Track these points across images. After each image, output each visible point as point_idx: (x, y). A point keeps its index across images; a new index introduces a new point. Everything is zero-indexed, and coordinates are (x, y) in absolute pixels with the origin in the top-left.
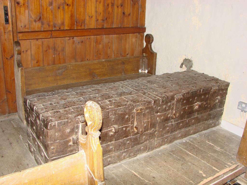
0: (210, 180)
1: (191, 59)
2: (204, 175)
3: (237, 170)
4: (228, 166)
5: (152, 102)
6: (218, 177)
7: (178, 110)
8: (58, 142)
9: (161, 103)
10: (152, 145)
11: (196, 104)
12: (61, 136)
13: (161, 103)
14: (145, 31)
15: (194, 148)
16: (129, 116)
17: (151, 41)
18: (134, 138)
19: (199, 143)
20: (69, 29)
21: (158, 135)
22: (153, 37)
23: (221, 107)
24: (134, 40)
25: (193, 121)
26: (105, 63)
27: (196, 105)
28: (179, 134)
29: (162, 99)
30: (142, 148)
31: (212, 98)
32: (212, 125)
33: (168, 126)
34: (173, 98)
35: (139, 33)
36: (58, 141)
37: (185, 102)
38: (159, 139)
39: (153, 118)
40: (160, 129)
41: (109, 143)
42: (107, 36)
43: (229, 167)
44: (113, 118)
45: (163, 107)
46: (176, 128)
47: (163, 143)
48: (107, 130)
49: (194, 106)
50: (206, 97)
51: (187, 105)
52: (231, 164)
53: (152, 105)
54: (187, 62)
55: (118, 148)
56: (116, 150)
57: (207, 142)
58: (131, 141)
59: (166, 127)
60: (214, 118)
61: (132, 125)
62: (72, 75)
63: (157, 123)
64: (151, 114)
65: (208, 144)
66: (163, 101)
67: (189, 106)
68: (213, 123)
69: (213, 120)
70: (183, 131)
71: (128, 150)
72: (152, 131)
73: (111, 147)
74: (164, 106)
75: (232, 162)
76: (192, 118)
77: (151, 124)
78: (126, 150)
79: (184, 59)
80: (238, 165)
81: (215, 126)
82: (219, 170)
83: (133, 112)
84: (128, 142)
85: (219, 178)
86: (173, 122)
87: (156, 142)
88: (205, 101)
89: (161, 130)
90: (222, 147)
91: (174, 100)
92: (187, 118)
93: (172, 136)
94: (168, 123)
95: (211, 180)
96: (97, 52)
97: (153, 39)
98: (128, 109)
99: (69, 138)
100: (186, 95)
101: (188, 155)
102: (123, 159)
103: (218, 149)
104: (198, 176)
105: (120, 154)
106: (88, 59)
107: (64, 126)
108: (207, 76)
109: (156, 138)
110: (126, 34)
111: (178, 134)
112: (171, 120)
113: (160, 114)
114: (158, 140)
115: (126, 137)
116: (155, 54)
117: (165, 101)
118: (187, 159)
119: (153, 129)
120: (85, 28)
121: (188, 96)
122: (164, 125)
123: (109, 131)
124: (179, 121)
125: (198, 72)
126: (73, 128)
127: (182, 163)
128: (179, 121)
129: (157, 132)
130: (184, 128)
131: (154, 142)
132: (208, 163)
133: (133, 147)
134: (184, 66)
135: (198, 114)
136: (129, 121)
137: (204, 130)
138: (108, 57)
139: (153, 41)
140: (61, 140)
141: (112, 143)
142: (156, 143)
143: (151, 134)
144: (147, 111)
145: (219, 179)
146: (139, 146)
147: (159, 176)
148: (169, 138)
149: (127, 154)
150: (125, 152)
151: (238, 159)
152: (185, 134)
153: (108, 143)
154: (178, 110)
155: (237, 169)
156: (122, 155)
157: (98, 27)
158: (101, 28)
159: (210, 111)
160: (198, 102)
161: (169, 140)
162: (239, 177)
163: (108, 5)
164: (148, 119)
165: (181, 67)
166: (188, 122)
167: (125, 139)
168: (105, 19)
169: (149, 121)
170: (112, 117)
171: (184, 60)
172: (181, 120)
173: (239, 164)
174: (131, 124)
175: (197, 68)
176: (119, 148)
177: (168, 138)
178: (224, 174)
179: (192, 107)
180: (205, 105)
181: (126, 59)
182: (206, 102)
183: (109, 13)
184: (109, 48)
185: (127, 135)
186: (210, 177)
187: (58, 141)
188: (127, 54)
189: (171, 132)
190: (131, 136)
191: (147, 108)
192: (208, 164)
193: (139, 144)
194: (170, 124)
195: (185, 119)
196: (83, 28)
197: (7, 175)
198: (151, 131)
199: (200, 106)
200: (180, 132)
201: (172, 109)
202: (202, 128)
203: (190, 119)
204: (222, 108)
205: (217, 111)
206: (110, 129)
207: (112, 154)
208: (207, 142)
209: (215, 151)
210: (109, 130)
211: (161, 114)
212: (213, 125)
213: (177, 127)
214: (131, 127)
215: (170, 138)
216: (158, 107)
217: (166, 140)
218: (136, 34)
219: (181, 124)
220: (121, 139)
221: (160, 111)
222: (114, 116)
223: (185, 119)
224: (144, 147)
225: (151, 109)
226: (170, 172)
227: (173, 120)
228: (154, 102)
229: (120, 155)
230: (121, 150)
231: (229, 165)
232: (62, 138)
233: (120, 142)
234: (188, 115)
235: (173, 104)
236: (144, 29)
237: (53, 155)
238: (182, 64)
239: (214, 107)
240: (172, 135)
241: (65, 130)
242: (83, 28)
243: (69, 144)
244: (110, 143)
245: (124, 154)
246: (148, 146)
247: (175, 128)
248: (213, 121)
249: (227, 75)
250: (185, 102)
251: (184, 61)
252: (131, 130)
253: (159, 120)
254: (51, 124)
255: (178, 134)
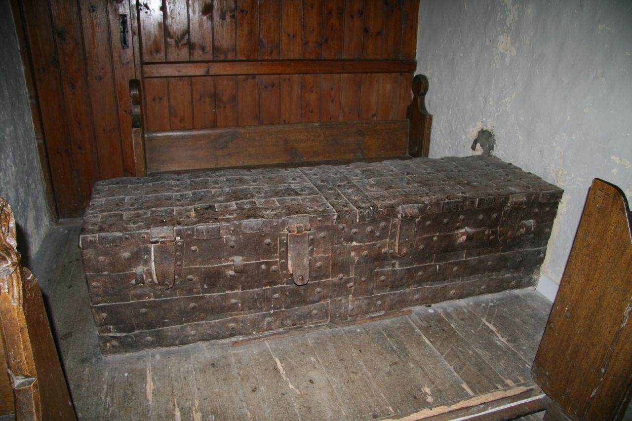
0: (439, 415)
1: (492, 130)
2: (430, 399)
3: (536, 397)
4: (503, 388)
5: (334, 215)
6: (467, 408)
7: (407, 239)
8: (105, 275)
9: (358, 220)
10: (342, 309)
11: (463, 231)
12: (112, 264)
13: (359, 221)
14: (414, 69)
15: (444, 330)
16: (274, 239)
17: (422, 91)
18: (290, 289)
19: (463, 320)
20: (244, 58)
21: (355, 290)
22: (427, 83)
23: (539, 245)
24: (388, 87)
25: (455, 269)
26: (319, 130)
27: (463, 234)
28: (417, 294)
29: (361, 212)
30: (315, 312)
31: (510, 222)
32: (510, 282)
33: (382, 274)
34: (391, 212)
35: (401, 73)
36: (106, 273)
37: (428, 223)
38: (360, 299)
39: (338, 252)
40: (361, 277)
41: (227, 292)
42: (328, 76)
43: (505, 390)
44: (231, 241)
45: (365, 229)
46: (404, 281)
47: (370, 308)
48: (219, 265)
49: (456, 234)
50: (492, 218)
51: (436, 233)
52: (513, 384)
53: (332, 222)
54: (485, 138)
55: (252, 304)
56: (247, 309)
57: (484, 320)
58: (284, 294)
59: (378, 275)
60: (517, 268)
61: (283, 261)
62: (246, 150)
63: (352, 263)
64: (332, 243)
65: (483, 326)
66: (362, 218)
67: (442, 234)
68: (513, 278)
69: (514, 272)
70: (426, 289)
71: (277, 312)
72: (338, 278)
73: (233, 301)
74: (369, 229)
75: (520, 378)
76: (450, 261)
77: (334, 265)
78: (273, 311)
79: (480, 130)
80: (532, 390)
81: (519, 286)
82: (473, 390)
83: (282, 233)
84: (276, 295)
85: (470, 411)
86: (397, 266)
87: (352, 305)
88: (490, 227)
89: (363, 279)
90: (514, 340)
91: (396, 216)
92: (437, 261)
93: (397, 296)
94: (383, 267)
95: (440, 413)
96: (306, 107)
97: (426, 85)
98: (269, 226)
99: (131, 271)
100: (430, 209)
101: (420, 343)
102: (265, 328)
103: (501, 340)
104: (415, 398)
105: (257, 318)
106: (284, 121)
107: (114, 245)
108: (516, 170)
109: (351, 296)
110: (371, 73)
111: (413, 293)
112: (391, 260)
113: (358, 244)
114: (357, 300)
115: (270, 284)
116: (428, 117)
117: (369, 218)
118: (414, 351)
119: (341, 275)
120: (278, 58)
121: (436, 211)
122: (372, 270)
123: (225, 266)
124: (415, 266)
125: (504, 160)
126: (137, 251)
127: (397, 360)
128: (414, 264)
129: (351, 284)
130: (429, 283)
131: (347, 304)
132: (458, 373)
133: (290, 308)
134: (478, 145)
135: (469, 254)
136: (275, 251)
137: (490, 291)
138: (331, 119)
139: (426, 89)
140: (113, 272)
141: (234, 294)
142: (351, 307)
143: (336, 285)
144: (322, 234)
145: (471, 414)
146: (305, 309)
147: (324, 380)
148: (388, 299)
149: (275, 321)
150: (270, 315)
151: (534, 374)
152: (432, 296)
153: (224, 291)
154: (407, 239)
155: (529, 397)
156: (262, 321)
157: (308, 56)
158: (314, 58)
159: (503, 251)
160: (468, 226)
161: (387, 303)
162: (530, 416)
163: (330, 13)
164: (325, 252)
165: (473, 148)
166: (439, 270)
167: (269, 289)
168: (323, 41)
169: (329, 257)
170: (229, 238)
171: (479, 132)
172: (419, 264)
173: (535, 386)
174: (281, 258)
175: (501, 152)
176: (253, 305)
177: (384, 300)
178: (486, 404)
179: (452, 239)
180: (489, 236)
181: (367, 125)
182: (492, 229)
183: (332, 30)
184: (333, 101)
185: (271, 280)
186: (443, 405)
187: (106, 273)
188: (374, 116)
189: (392, 288)
190: (284, 284)
191: (320, 229)
192: (455, 374)
193: (307, 304)
194: (388, 268)
195: (433, 263)
196: (273, 59)
197: (387, 317)
198: (336, 279)
199: (470, 238)
200: (418, 290)
201: (393, 236)
202: (483, 287)
203: (444, 264)
204: (541, 248)
205: (525, 253)
206: (226, 264)
207: (237, 315)
208: (484, 320)
209: (490, 345)
210: (223, 264)
211: (361, 244)
212: (513, 283)
213: (409, 278)
214: (280, 265)
215: (390, 300)
216: (351, 229)
217: (379, 302)
218: (393, 75)
219: (420, 273)
220: (258, 287)
221: (359, 237)
222: (234, 237)
223: (433, 263)
224: (320, 310)
225: (334, 232)
226: (355, 377)
227: (397, 262)
228: (339, 217)
229: (258, 320)
230: (261, 309)
231: (508, 385)
232: (113, 267)
233: (253, 292)
234: (439, 256)
235: (394, 226)
236: (413, 65)
237: (100, 298)
238: (475, 142)
239: (517, 242)
240: (395, 294)
241: (118, 254)
242: (275, 57)
243: (131, 282)
244: (230, 292)
245: (268, 319)
246: (330, 311)
247: (402, 279)
248: (515, 275)
249: (560, 172)
250: (428, 223)
251: (480, 134)
252: (282, 272)
253: (357, 258)
254: (84, 237)
255: (413, 293)
